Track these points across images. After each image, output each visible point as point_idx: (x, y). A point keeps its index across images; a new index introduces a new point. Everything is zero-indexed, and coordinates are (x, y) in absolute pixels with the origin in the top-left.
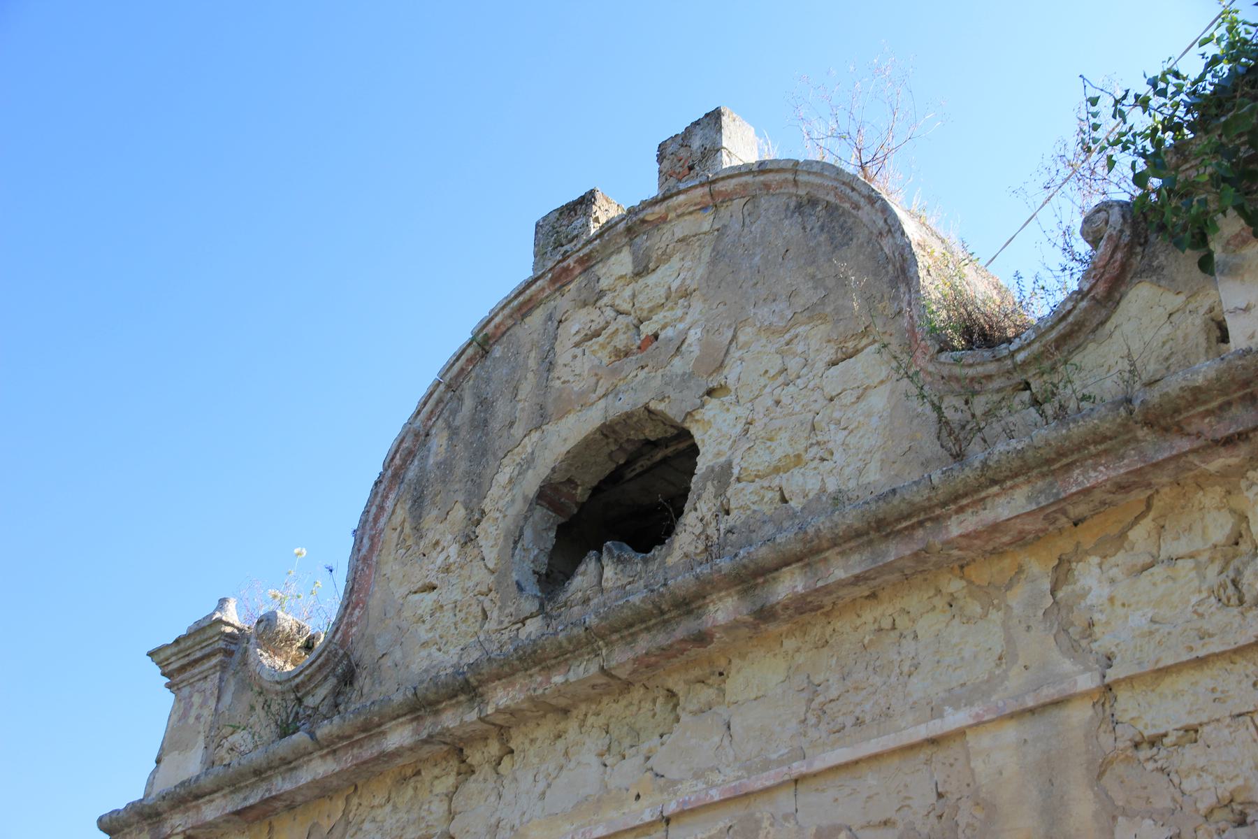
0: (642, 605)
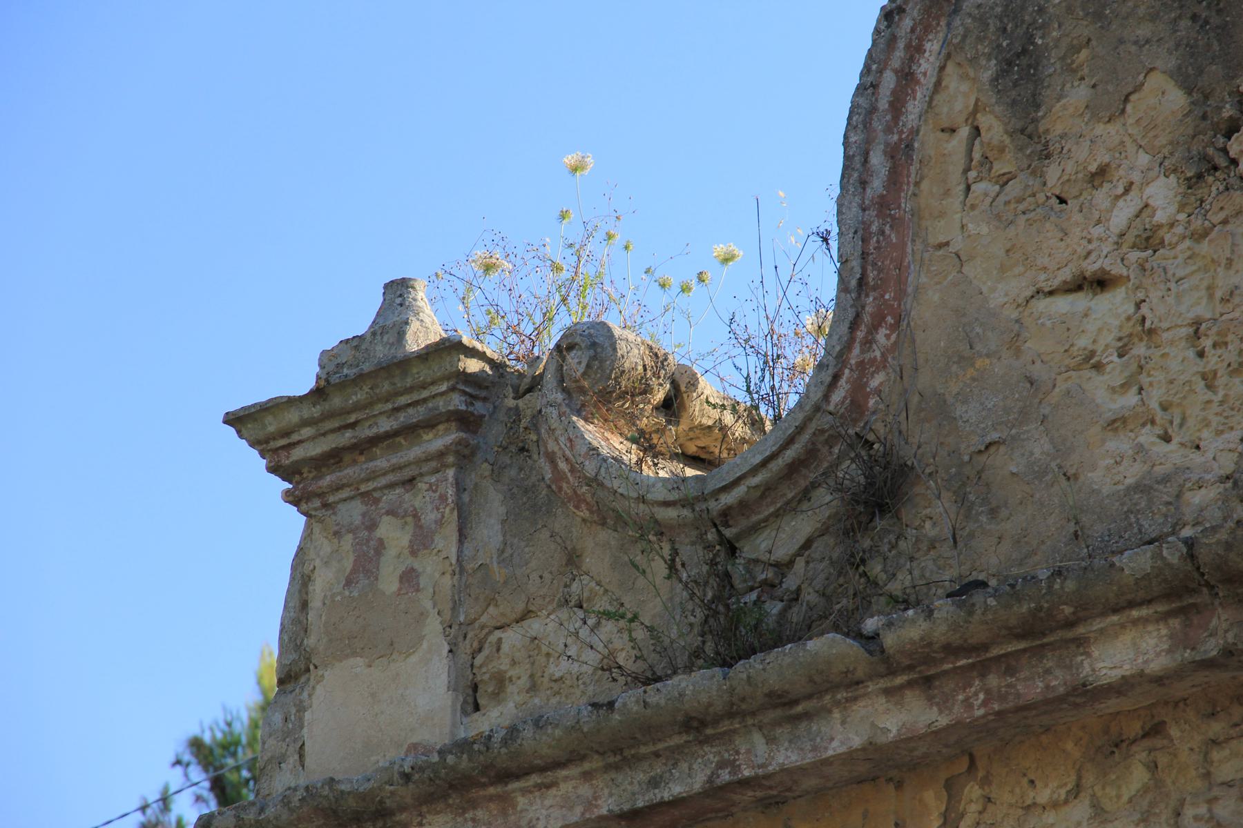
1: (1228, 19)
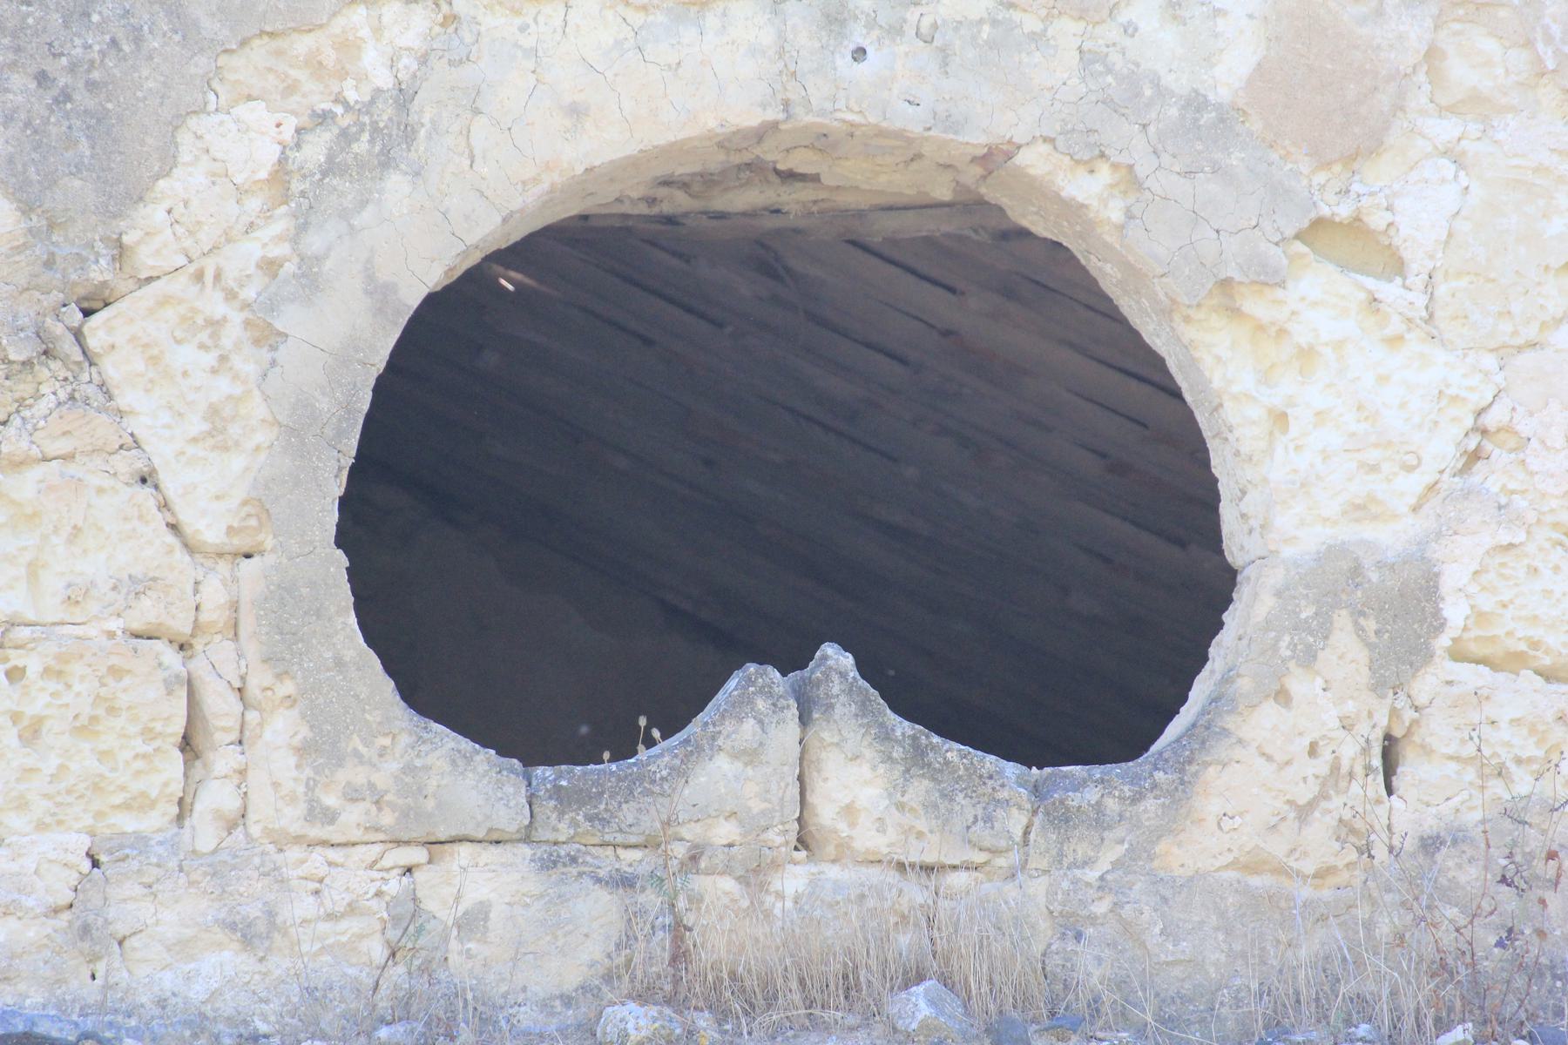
1: (110, 106)
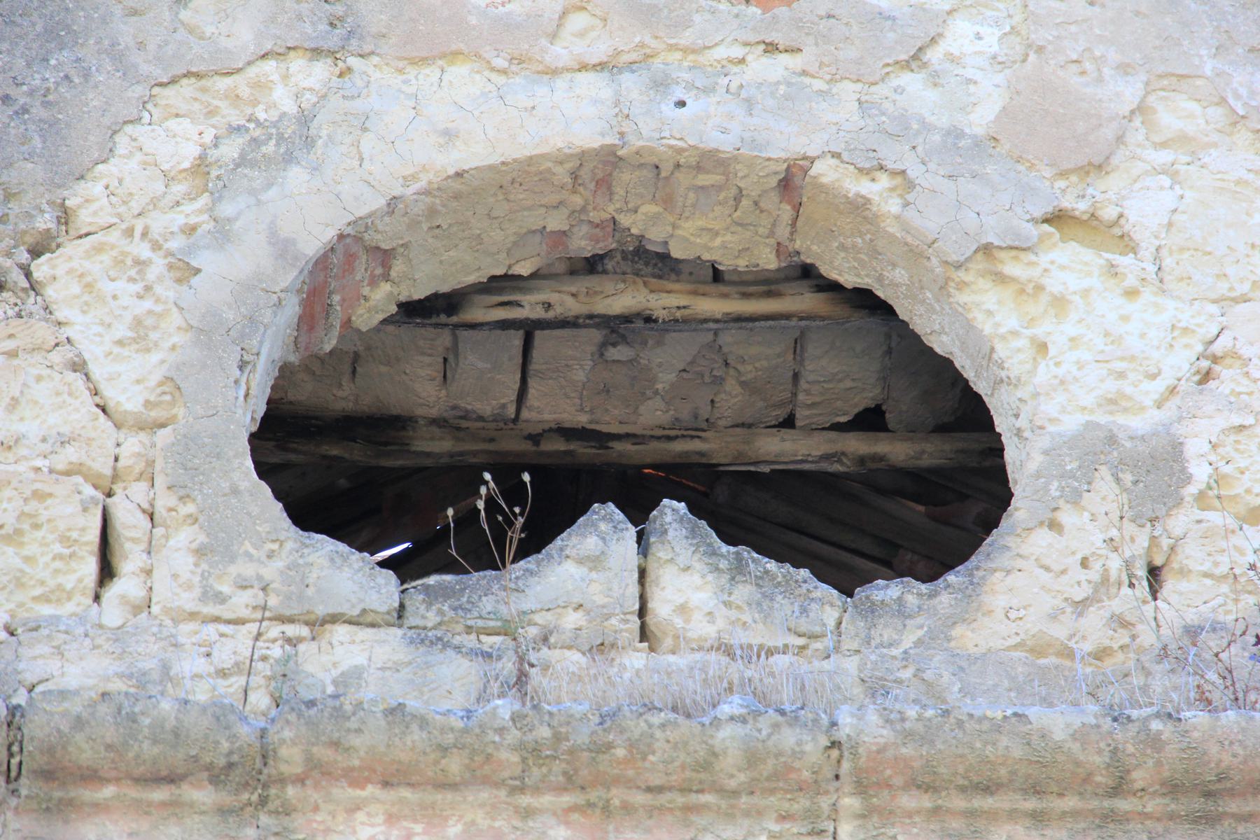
0: (1076, 747)
1: (60, 116)
